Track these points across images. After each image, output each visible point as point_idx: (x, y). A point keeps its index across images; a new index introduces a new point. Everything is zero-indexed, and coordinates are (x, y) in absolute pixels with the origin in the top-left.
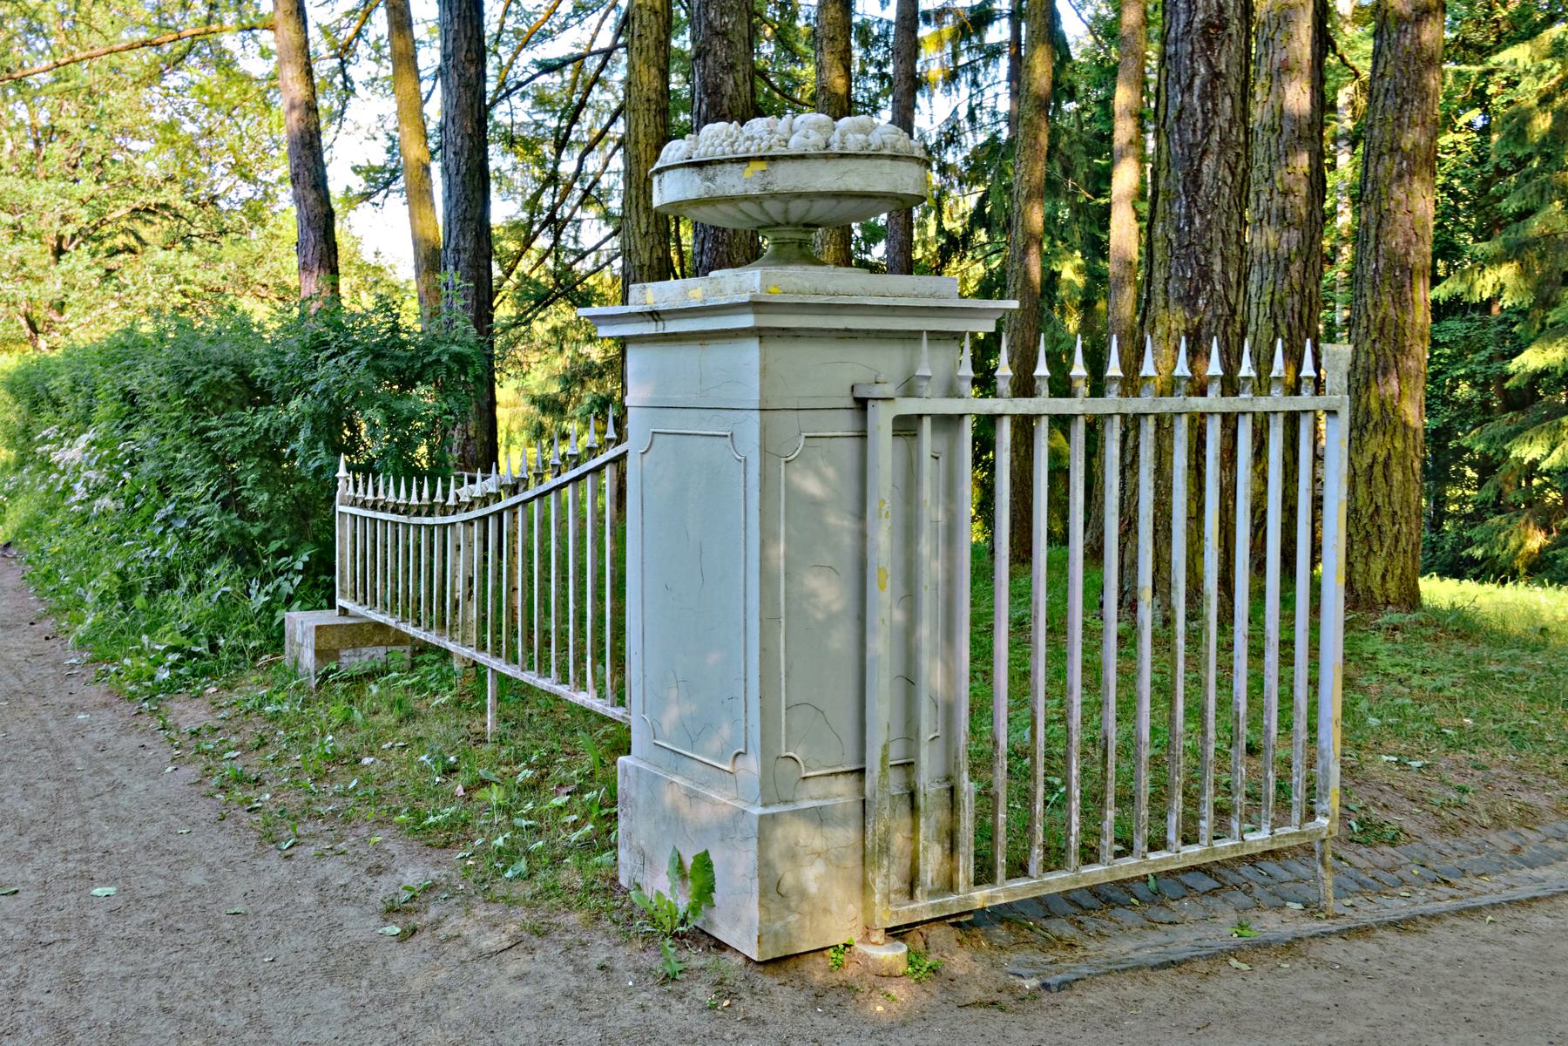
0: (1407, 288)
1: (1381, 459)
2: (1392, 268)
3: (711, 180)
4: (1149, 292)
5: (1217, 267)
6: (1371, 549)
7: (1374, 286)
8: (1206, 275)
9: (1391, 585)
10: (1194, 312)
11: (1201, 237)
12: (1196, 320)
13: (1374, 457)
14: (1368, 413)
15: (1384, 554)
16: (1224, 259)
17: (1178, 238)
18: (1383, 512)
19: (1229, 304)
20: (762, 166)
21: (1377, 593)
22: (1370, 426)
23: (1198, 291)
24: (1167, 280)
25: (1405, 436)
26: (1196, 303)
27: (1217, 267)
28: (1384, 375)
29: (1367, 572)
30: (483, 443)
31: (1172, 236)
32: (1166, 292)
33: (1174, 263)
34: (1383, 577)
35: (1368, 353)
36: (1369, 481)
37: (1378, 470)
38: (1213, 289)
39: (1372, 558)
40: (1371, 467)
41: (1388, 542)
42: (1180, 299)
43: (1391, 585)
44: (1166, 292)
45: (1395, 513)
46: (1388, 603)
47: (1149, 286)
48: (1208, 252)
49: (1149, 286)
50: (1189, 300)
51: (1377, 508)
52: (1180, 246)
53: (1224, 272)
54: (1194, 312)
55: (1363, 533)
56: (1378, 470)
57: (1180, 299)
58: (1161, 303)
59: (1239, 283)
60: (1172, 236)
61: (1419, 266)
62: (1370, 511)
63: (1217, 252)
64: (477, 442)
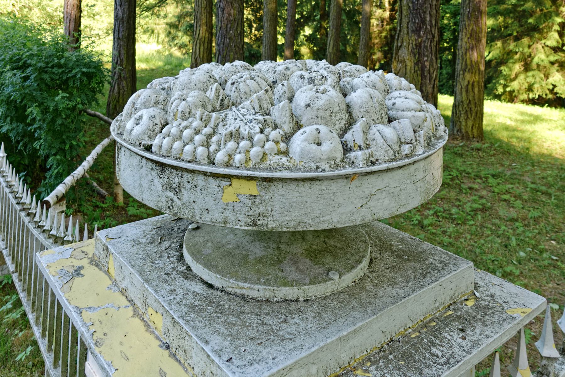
0: (479, 19)
1: (471, 83)
2: (475, 11)
3: (177, 190)
4: (400, 27)
5: (428, 19)
6: (468, 117)
7: (468, 17)
8: (423, 22)
9: (475, 131)
10: (419, 36)
11: (422, 6)
12: (420, 40)
13: (469, 82)
14: (466, 65)
15: (472, 118)
16: (431, 15)
17: (413, 6)
18: (472, 102)
19: (432, 34)
20: (253, 188)
21: (470, 133)
22: (467, 70)
23: (420, 28)
24: (408, 23)
25: (479, 74)
26: (420, 33)
27: (428, 19)
28: (472, 51)
29: (466, 125)
30: (129, 70)
31: (411, 5)
32: (408, 27)
33: (411, 16)
34: (472, 127)
35: (466, 42)
36: (467, 91)
37: (470, 87)
38: (426, 28)
39: (468, 120)
40: (468, 85)
41: (473, 115)
42: (413, 31)
43: (475, 131)
44: (408, 27)
45: (476, 103)
46: (474, 137)
47: (400, 24)
48: (425, 12)
49: (400, 24)
50: (417, 31)
51: (470, 101)
52: (414, 8)
53: (431, 21)
54: (419, 36)
55: (465, 111)
56: (470, 87)
57: (413, 31)
58: (406, 32)
59: (435, 25)
60: (411, 5)
61: (483, 11)
62: (468, 102)
63: (428, 12)
64: (127, 70)
